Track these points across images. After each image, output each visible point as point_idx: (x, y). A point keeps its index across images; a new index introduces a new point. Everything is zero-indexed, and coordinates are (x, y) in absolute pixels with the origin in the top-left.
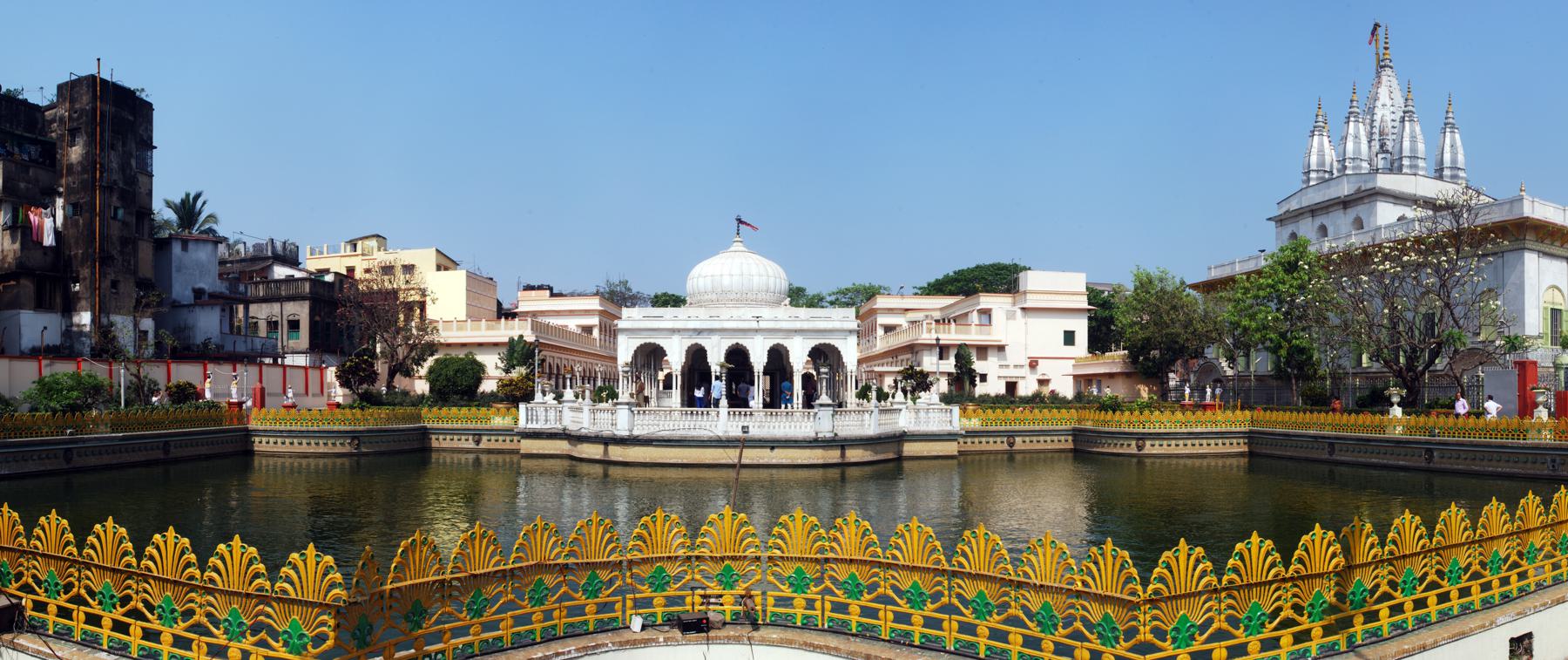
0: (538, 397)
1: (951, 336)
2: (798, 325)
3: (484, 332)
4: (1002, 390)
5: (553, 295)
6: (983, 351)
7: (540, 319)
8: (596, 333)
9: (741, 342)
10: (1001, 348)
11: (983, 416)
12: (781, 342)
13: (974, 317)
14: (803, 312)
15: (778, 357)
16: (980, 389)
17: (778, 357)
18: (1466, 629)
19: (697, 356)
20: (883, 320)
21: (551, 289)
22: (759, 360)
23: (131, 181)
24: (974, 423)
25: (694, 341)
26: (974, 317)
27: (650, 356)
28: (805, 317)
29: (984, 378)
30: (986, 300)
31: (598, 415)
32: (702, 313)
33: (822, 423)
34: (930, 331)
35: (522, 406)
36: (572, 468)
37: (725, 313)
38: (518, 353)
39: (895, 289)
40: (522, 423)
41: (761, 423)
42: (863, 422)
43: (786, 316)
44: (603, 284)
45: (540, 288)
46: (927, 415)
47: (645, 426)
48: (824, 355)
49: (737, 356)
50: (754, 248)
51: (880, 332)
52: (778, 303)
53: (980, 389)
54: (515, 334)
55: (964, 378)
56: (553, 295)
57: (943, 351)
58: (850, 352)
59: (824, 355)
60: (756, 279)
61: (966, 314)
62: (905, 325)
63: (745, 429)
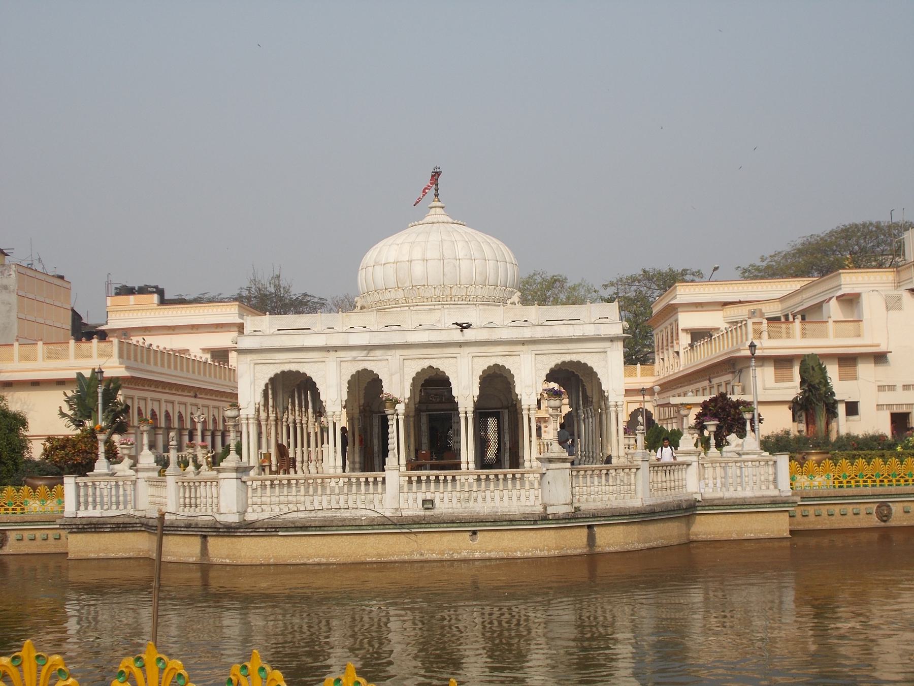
0: (101, 465)
1: (796, 341)
2: (527, 333)
3: (40, 363)
4: (885, 428)
5: (163, 302)
6: (848, 360)
7: (134, 340)
9: (436, 364)
10: (880, 358)
11: (834, 471)
12: (500, 361)
13: (834, 310)
14: (534, 312)
15: (497, 384)
16: (844, 426)
17: (497, 384)
19: (367, 391)
20: (688, 320)
21: (161, 292)
22: (466, 392)
23: (778, 275)
24: (820, 482)
25: (360, 366)
26: (834, 310)
27: (294, 389)
29: (852, 409)
30: (851, 281)
32: (371, 319)
35: (69, 482)
36: (150, 581)
37: (409, 319)
38: (88, 395)
39: (707, 272)
40: (70, 508)
41: (466, 492)
42: (632, 482)
45: (142, 291)
46: (742, 480)
47: (268, 505)
48: (573, 381)
49: (433, 387)
50: (464, 216)
51: (685, 340)
53: (844, 426)
54: (95, 362)
55: (815, 401)
56: (163, 302)
57: (782, 362)
58: (614, 376)
60: (465, 265)
61: (818, 307)
63: (428, 504)
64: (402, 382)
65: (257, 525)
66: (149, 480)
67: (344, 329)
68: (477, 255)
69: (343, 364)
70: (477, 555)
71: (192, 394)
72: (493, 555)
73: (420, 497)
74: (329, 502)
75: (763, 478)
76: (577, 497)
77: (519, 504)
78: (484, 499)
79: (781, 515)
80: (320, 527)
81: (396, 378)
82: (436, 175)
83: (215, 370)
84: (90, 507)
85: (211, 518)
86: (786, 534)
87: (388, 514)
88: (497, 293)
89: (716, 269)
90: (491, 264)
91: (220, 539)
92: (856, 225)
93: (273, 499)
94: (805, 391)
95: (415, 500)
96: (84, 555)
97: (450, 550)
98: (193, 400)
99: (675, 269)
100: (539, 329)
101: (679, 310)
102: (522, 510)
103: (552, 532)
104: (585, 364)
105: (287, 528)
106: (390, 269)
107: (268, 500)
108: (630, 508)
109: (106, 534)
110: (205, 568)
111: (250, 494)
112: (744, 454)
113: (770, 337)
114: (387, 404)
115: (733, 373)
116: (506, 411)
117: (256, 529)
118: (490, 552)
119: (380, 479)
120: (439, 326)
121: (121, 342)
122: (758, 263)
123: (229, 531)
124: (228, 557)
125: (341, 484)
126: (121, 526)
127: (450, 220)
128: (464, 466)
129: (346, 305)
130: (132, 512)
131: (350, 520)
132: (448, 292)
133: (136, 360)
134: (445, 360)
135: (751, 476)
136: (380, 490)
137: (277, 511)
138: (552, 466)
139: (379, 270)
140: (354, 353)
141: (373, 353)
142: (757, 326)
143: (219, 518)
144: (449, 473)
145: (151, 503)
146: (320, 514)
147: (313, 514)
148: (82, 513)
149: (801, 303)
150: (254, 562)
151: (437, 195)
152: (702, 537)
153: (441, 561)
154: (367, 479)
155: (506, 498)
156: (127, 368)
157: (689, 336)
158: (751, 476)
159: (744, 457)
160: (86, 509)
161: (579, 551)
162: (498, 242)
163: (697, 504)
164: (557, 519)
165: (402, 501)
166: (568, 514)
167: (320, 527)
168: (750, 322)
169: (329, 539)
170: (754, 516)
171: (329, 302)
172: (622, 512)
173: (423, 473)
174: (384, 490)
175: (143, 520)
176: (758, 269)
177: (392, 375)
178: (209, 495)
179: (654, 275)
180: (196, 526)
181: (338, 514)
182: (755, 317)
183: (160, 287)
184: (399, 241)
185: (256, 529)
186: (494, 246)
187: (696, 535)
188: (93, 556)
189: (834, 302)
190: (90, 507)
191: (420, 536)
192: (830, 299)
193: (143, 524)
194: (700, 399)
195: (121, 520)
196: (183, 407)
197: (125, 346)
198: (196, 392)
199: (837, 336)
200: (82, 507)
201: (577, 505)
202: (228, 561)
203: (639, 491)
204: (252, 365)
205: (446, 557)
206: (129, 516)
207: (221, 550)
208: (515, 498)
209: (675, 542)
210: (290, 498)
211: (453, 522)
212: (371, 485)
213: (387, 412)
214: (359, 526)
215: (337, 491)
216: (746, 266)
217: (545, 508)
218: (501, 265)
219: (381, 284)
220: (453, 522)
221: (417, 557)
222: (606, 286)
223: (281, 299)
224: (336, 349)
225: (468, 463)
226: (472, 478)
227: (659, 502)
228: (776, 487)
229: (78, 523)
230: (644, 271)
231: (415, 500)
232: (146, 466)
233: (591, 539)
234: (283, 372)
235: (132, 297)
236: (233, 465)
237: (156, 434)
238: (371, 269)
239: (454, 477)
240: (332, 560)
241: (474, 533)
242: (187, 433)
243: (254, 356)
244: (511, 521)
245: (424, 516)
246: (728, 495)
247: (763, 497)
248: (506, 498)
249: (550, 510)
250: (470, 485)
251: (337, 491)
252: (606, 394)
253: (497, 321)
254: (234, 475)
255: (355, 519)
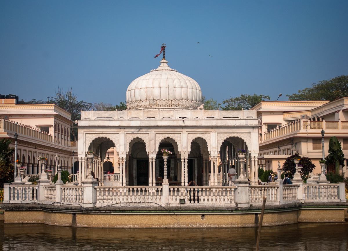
0: (18, 180)
2: (214, 123)
5: (18, 103)
8: (51, 131)
9: (171, 136)
12: (201, 136)
15: (199, 147)
17: (199, 147)
18: (127, 178)
19: (137, 147)
21: (17, 98)
25: (135, 136)
28: (218, 116)
31: (68, 192)
32: (141, 114)
33: (243, 197)
34: (305, 127)
37: (159, 115)
43: (201, 116)
44: (55, 96)
45: (8, 97)
48: (233, 147)
50: (176, 67)
52: (195, 108)
56: (18, 103)
58: (253, 142)
59: (233, 147)
60: (178, 90)
61: (333, 114)
62: (284, 124)
64: (155, 144)
65: (102, 209)
66: (45, 187)
67: (128, 118)
68: (184, 85)
69: (189, 135)
70: (204, 226)
71: (34, 147)
72: (212, 226)
73: (178, 198)
74: (135, 199)
75: (329, 194)
76: (251, 200)
77: (224, 202)
78: (208, 200)
79: (341, 212)
80: (131, 211)
81: (152, 142)
82: (164, 47)
83: (44, 136)
84: (16, 199)
85: (78, 205)
86: (343, 220)
87: (163, 205)
88: (192, 104)
89: (280, 95)
90: (190, 90)
91: (82, 215)
92: (345, 76)
93: (109, 197)
94: (331, 154)
95: (176, 199)
96: (12, 222)
97: (192, 223)
98: (35, 150)
99: (257, 95)
100: (219, 121)
101: (262, 114)
102: (226, 205)
103: (239, 216)
104: (109, 139)
105: (115, 211)
106: (143, 91)
107: (107, 198)
108: (274, 206)
109: (23, 212)
110: (74, 228)
111: (98, 195)
112: (320, 182)
113: (311, 128)
114: (164, 154)
115: (292, 144)
116: (196, 159)
117: (100, 211)
118: (210, 224)
119: (159, 189)
120: (173, 118)
121: (5, 121)
122: (298, 93)
123: (87, 211)
124: (86, 224)
125: (125, 191)
126: (30, 208)
127: (171, 69)
128: (183, 184)
129: (122, 107)
130: (36, 202)
131: (145, 208)
132: (170, 103)
133: (11, 130)
134: (175, 135)
135: (323, 193)
136: (159, 194)
137: (110, 203)
138: (241, 185)
139: (137, 91)
140: (133, 130)
141: (141, 130)
142: (305, 123)
143: (82, 205)
144: (143, 187)
145: (46, 197)
146: (131, 205)
147: (128, 205)
148: (12, 202)
149: (322, 112)
150: (99, 226)
151: (164, 57)
152: (304, 220)
153: (187, 228)
154: (137, 189)
155: (218, 200)
156: (8, 134)
157: (267, 127)
158: (323, 193)
159: (320, 184)
160: (14, 199)
161: (251, 225)
162: (193, 80)
163: (302, 205)
164: (242, 210)
165: (170, 200)
166: (247, 208)
167: (131, 211)
168: (302, 121)
169: (135, 217)
170: (328, 211)
171: (93, 105)
172: (271, 207)
173: (135, 187)
174: (162, 194)
175: (42, 206)
176: (297, 96)
177: (150, 141)
178: (78, 194)
179: (247, 98)
180: (71, 209)
181: (140, 205)
182: (304, 118)
183: (17, 96)
184: (147, 78)
185: (100, 211)
186: (191, 82)
187: (301, 219)
188: (16, 222)
189: (341, 112)
190: (16, 199)
191: (178, 216)
192: (340, 110)
193: (41, 208)
194: (286, 156)
195: (31, 205)
196: (35, 154)
197: (7, 123)
198: (36, 146)
199: (342, 129)
200: (12, 199)
201: (251, 204)
202: (86, 226)
203: (276, 196)
204: (84, 134)
205: (190, 226)
206: (35, 203)
207: (82, 220)
208: (222, 200)
209: (292, 222)
210: (104, 197)
211: (194, 210)
212: (139, 192)
213: (164, 158)
214: (150, 211)
215: (123, 194)
216: (291, 95)
217: (237, 205)
218: (195, 91)
219: (138, 98)
220: (194, 210)
221: (176, 226)
222: (224, 102)
223: (71, 103)
224: (124, 128)
225: (185, 183)
226: (154, 190)
227: (286, 203)
228: (338, 198)
229: (10, 206)
230: (242, 96)
231: (176, 199)
232: (44, 180)
233: (74, 220)
234: (99, 138)
235: (3, 100)
236: (91, 180)
237: (29, 166)
238: (133, 91)
239: (178, 189)
240: (136, 226)
241: (203, 215)
242: (31, 165)
243: (189, 130)
244: (221, 210)
245: (181, 207)
246: (316, 201)
247: (332, 202)
248: (218, 200)
249: (239, 206)
250: (153, 193)
251: (123, 194)
252: (209, 153)
253: (200, 117)
254: (91, 185)
255: (148, 208)
